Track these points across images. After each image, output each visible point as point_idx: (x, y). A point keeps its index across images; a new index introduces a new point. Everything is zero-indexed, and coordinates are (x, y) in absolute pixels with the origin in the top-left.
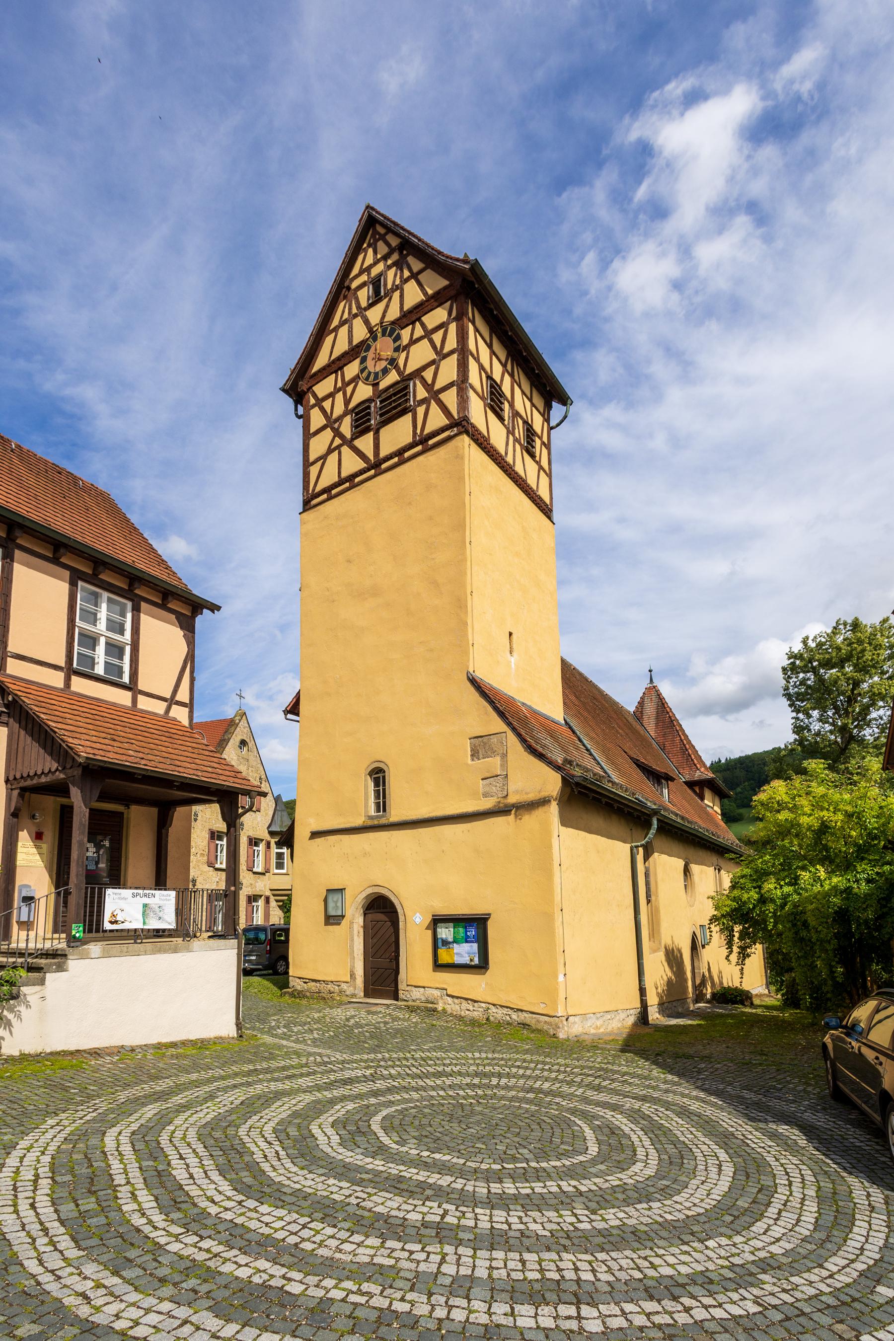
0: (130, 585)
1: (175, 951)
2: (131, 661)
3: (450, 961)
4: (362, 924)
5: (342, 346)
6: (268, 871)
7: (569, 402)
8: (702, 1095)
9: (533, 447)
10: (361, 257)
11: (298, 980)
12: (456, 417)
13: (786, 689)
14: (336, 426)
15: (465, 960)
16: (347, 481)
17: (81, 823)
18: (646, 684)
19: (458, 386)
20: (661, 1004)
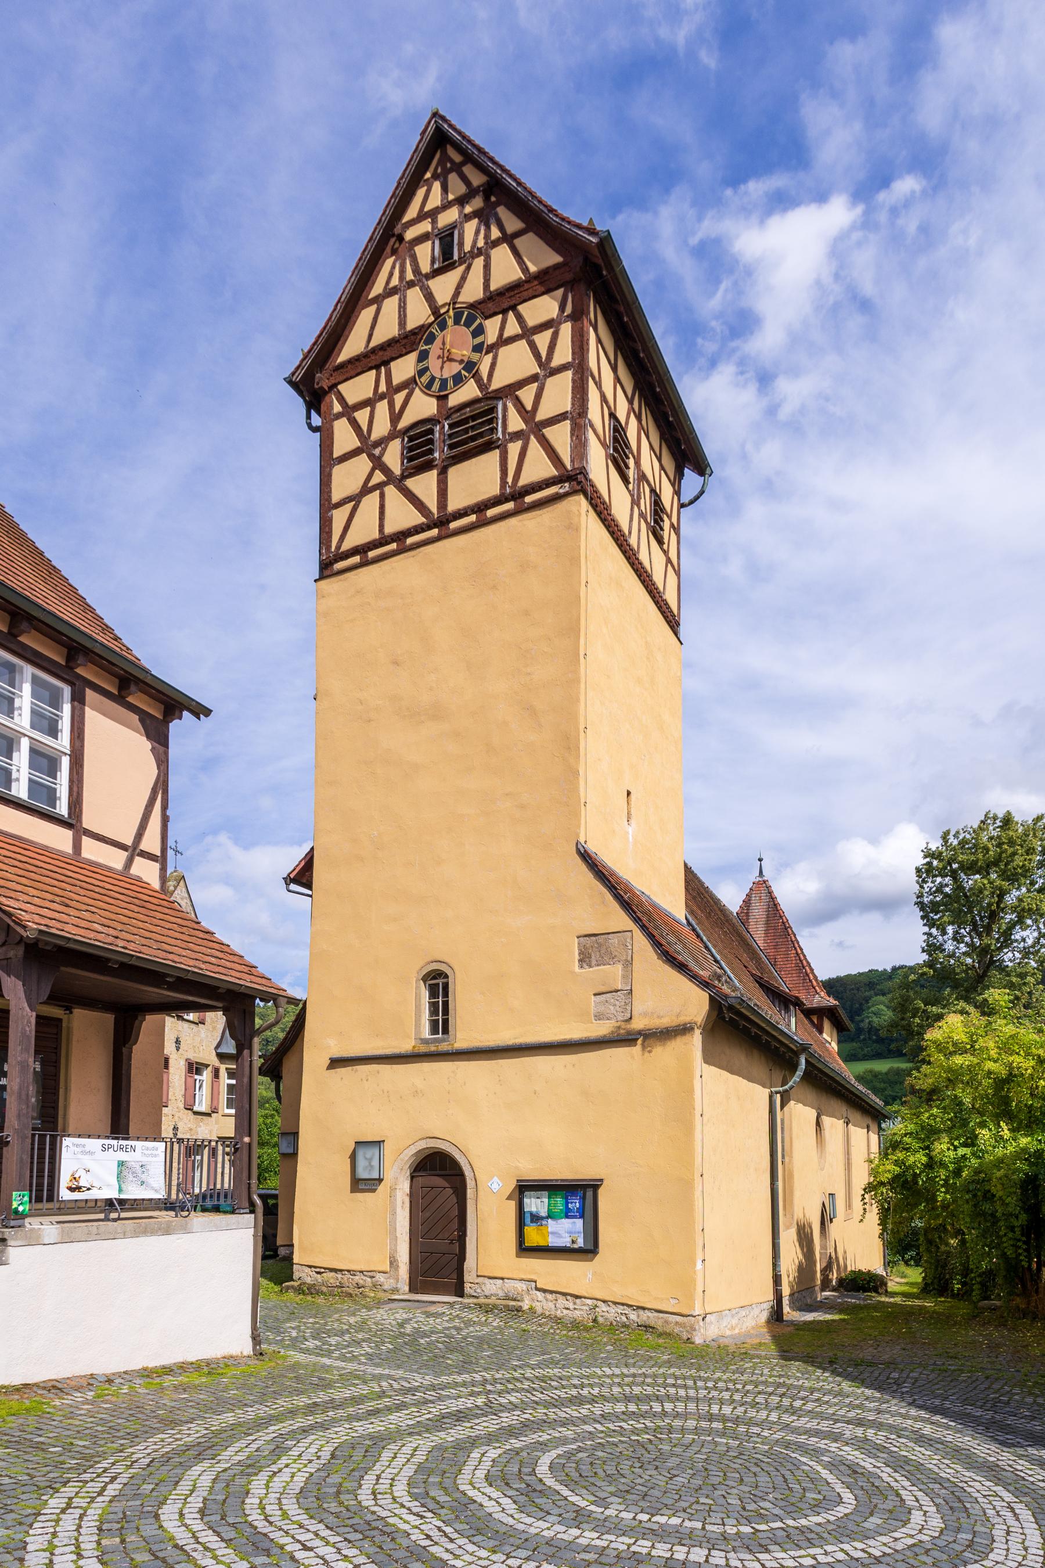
0: (70, 658)
1: (167, 1231)
2: (71, 781)
3: (542, 1243)
4: (408, 1191)
5: (388, 329)
6: (215, 1111)
7: (708, 471)
8: (922, 1413)
9: (662, 529)
10: (421, 193)
11: (307, 1270)
12: (569, 468)
13: (920, 896)
14: (377, 452)
15: (565, 1241)
16: (393, 541)
17: (24, 1033)
18: (754, 876)
19: (572, 420)
20: (791, 1295)
